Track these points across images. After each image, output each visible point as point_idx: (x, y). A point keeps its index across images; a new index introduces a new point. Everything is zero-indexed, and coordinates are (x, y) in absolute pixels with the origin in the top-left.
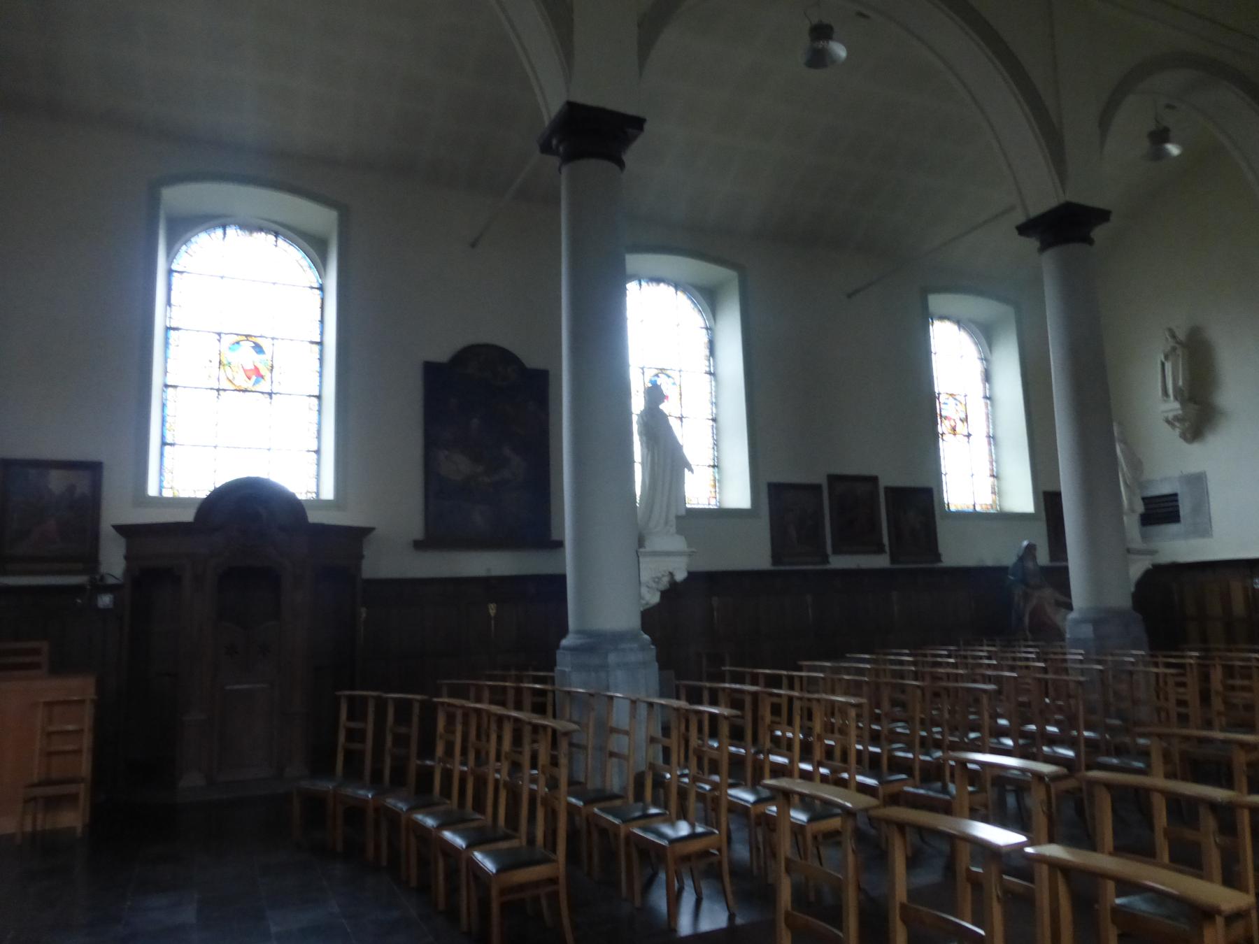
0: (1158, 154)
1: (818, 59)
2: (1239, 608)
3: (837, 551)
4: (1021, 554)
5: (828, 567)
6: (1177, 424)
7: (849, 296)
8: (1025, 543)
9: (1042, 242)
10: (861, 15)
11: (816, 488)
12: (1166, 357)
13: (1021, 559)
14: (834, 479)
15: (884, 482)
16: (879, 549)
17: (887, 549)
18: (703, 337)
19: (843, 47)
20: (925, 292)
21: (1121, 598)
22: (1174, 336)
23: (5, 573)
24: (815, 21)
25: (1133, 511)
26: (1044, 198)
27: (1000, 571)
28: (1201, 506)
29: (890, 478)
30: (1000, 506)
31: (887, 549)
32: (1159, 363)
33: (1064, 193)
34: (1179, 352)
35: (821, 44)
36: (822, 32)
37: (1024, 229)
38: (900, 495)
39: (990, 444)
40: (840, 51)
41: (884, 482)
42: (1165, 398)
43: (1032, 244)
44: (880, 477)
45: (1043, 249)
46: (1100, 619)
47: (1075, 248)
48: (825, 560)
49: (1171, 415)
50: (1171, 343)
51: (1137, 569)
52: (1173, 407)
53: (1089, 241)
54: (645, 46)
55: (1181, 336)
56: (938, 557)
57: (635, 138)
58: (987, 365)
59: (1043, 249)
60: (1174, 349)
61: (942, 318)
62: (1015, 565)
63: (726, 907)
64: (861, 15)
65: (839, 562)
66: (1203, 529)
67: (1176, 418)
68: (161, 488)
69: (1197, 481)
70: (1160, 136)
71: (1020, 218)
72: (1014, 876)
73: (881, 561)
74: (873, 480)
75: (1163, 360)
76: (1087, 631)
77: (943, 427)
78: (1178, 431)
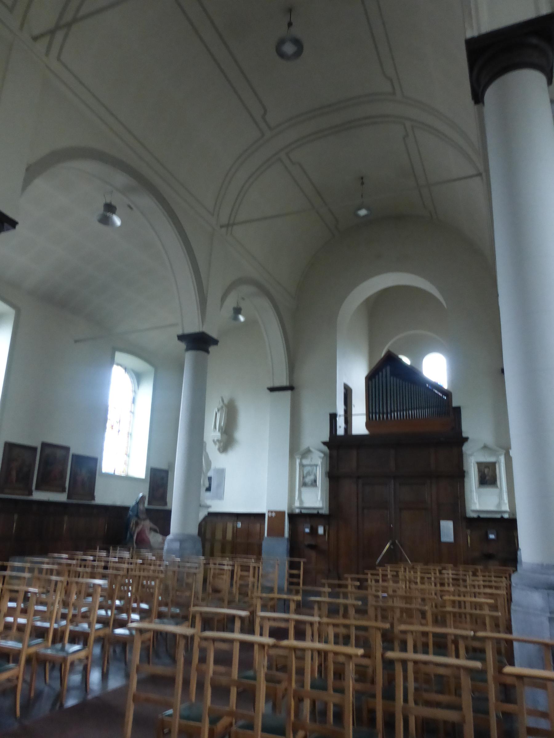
0: (236, 318)
1: (105, 220)
2: (229, 536)
3: (37, 488)
4: (138, 501)
5: (93, 502)
6: (217, 443)
7: (76, 341)
8: (141, 495)
9: (187, 346)
10: (130, 207)
11: (34, 449)
12: (218, 411)
13: (138, 503)
14: (45, 445)
15: (73, 451)
16: (63, 490)
17: (67, 490)
18: (131, 395)
19: (119, 219)
20: (115, 350)
21: (194, 530)
22: (223, 401)
23: (2, 492)
24: (108, 201)
25: (204, 485)
26: (193, 327)
27: (124, 510)
28: (221, 485)
29: (76, 449)
30: (127, 473)
31: (67, 490)
32: (215, 412)
33: (203, 326)
34: (224, 409)
35: (108, 214)
36: (110, 208)
37: (181, 338)
38: (79, 459)
39: (128, 437)
40: (117, 221)
41: (73, 451)
42: (214, 429)
43: (182, 345)
44: (71, 447)
45: (187, 349)
46: (182, 540)
47: (201, 353)
48: (30, 493)
49: (216, 439)
50: (221, 404)
51: (202, 514)
52: (217, 435)
53: (207, 352)
54: (27, 182)
55: (226, 401)
56: (93, 498)
57: (8, 230)
58: (135, 396)
59: (187, 349)
60: (222, 407)
61: (118, 364)
62: (134, 507)
63: (101, 671)
64: (130, 207)
65: (39, 496)
66: (220, 497)
67: (218, 440)
68: (301, 501)
69: (221, 472)
70: (238, 311)
71: (180, 332)
72: (470, 540)
73: (62, 497)
74: (67, 449)
75: (217, 411)
76: (177, 545)
77: (108, 425)
78: (217, 447)
